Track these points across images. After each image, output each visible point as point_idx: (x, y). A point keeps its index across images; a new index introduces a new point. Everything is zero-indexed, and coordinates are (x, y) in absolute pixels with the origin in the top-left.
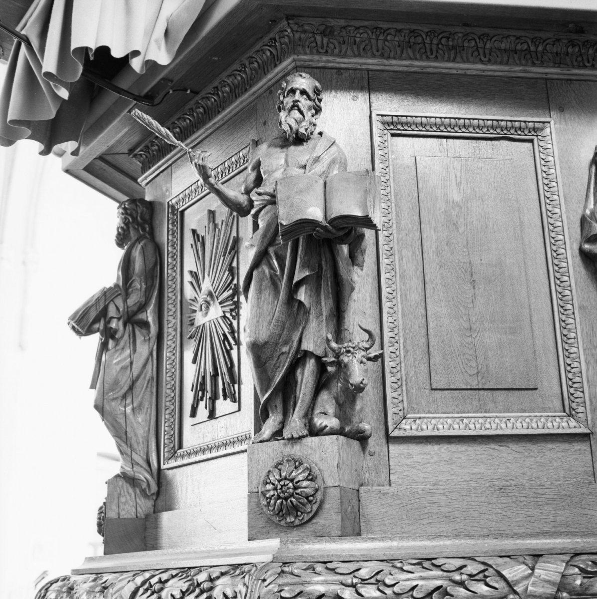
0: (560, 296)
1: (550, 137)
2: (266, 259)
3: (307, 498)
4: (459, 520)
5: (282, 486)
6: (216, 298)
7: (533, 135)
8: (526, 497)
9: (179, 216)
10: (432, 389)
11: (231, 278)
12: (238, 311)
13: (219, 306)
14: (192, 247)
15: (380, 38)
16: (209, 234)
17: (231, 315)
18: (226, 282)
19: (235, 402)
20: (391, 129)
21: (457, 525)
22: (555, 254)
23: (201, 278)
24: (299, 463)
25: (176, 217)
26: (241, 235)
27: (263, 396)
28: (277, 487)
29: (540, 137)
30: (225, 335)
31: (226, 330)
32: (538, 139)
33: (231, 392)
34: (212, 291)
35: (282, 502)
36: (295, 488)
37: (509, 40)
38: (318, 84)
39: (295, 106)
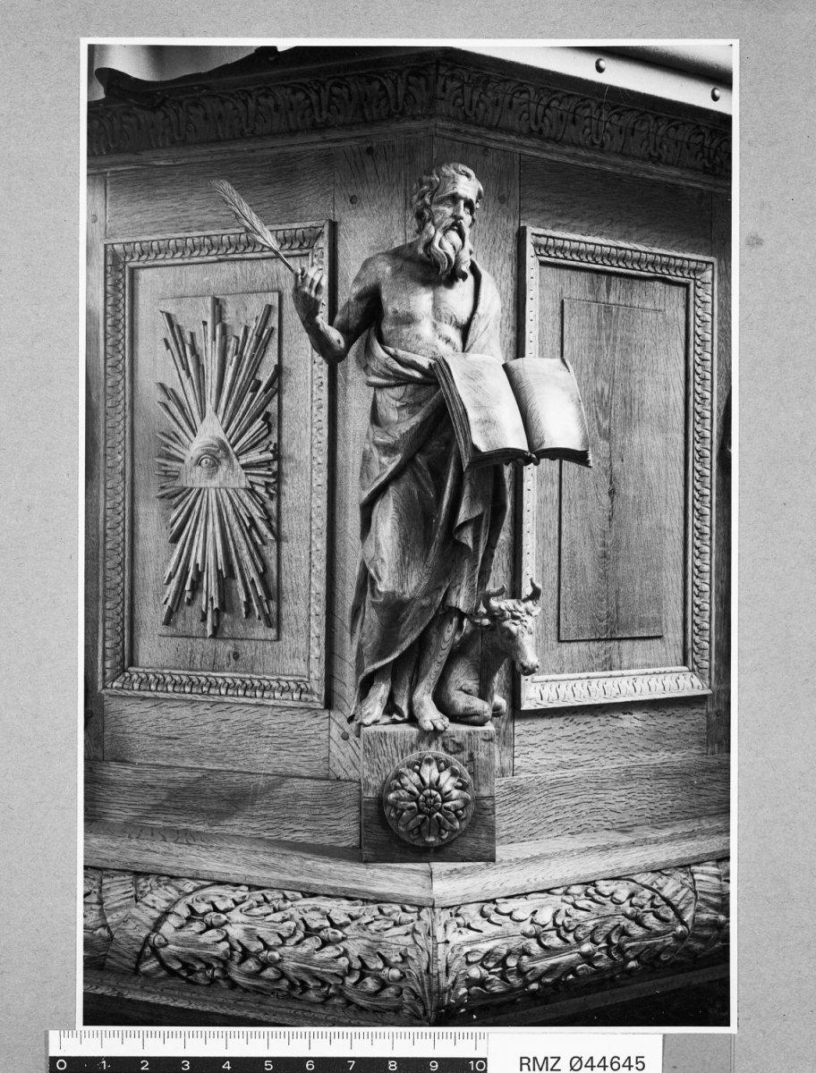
0: (697, 514)
1: (710, 286)
2: (410, 469)
3: (455, 812)
4: (584, 813)
5: (426, 797)
6: (234, 456)
7: (691, 278)
8: (648, 779)
9: (127, 275)
10: (560, 641)
11: (265, 433)
12: (279, 486)
13: (242, 472)
14: (168, 347)
15: (541, 103)
16: (214, 339)
17: (267, 492)
18: (258, 436)
19: (270, 626)
20: (542, 255)
21: (583, 820)
22: (697, 456)
23: (195, 409)
24: (445, 764)
25: (121, 276)
26: (285, 363)
27: (374, 662)
28: (418, 798)
29: (699, 283)
30: (251, 519)
31: (256, 514)
32: (695, 285)
33: (264, 611)
34: (226, 441)
35: (425, 818)
36: (444, 801)
37: (686, 128)
38: (482, 189)
39: (457, 226)
